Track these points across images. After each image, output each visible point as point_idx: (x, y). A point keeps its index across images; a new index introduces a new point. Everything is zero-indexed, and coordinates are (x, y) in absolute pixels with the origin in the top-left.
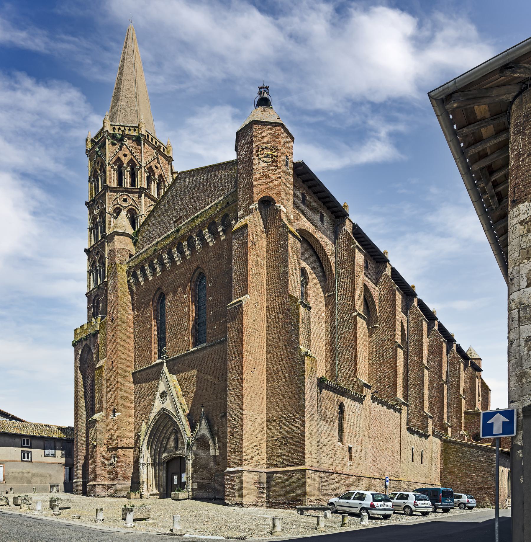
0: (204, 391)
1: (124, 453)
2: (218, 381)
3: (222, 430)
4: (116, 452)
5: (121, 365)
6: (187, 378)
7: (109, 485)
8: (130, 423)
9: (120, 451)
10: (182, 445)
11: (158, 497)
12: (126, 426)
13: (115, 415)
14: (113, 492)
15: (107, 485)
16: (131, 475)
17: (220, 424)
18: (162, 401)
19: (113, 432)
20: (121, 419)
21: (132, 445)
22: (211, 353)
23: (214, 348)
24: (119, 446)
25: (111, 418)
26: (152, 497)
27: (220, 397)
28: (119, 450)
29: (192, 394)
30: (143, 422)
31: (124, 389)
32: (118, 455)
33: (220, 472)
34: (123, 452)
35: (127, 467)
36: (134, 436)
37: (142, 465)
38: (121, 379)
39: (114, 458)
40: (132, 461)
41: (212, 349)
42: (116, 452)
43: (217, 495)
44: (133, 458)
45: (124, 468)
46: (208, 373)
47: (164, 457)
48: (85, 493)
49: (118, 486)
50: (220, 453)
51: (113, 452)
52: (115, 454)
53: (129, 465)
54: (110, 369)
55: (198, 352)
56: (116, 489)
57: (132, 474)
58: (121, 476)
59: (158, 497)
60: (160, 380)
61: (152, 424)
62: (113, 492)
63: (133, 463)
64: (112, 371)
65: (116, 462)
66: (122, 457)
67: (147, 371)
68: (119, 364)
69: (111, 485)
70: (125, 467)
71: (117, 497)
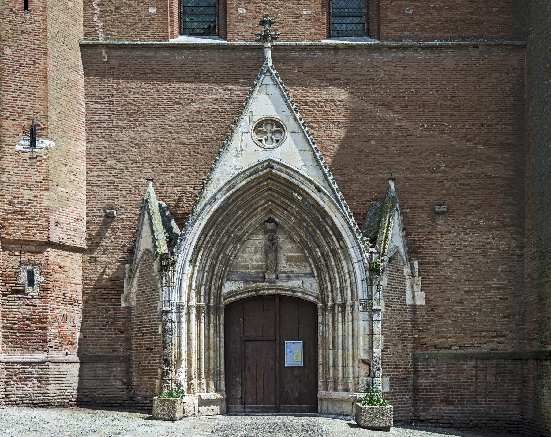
0: (373, 143)
1: (63, 264)
2: (421, 130)
3: (435, 246)
4: (41, 258)
5: (55, 12)
6: (313, 102)
7: (12, 363)
8: (78, 176)
9: (53, 255)
10: (290, 265)
11: (217, 409)
12: (68, 184)
13: (38, 145)
14: (31, 387)
15: (6, 363)
16: (78, 335)
17: (429, 229)
18: (261, 141)
19: (27, 194)
20: (56, 159)
21: (81, 243)
22: (398, 63)
23: (409, 54)
24: (54, 239)
25: (19, 148)
26: (203, 409)
27: (428, 166)
28: (51, 251)
29: (329, 143)
30: (151, 184)
31: (64, 79)
32: (46, 267)
33: (427, 349)
34: (59, 260)
35: (68, 308)
36: (85, 217)
37: (174, 307)
38: (55, 50)
39: (31, 274)
40: (80, 288)
41: (400, 54)
42: (37, 256)
43: (424, 410)
44: (80, 282)
45: (62, 310)
46: (388, 106)
47: (229, 293)
48: (207, 392)
49: (52, 369)
50: (427, 300)
51: (28, 255)
52: (33, 264)
53: (73, 302)
54: (14, 13)
55: (350, 52)
56: (43, 377)
57: (81, 331)
58: (54, 334)
59: (217, 409)
60: (257, 88)
61: (218, 196)
62: (31, 387)
63: (80, 297)
64: (22, 19)
65: (36, 289)
66: (56, 275)
67: (146, 53)
68: (50, 9)
69: (24, 363)
70: (63, 307)
71: (48, 405)
